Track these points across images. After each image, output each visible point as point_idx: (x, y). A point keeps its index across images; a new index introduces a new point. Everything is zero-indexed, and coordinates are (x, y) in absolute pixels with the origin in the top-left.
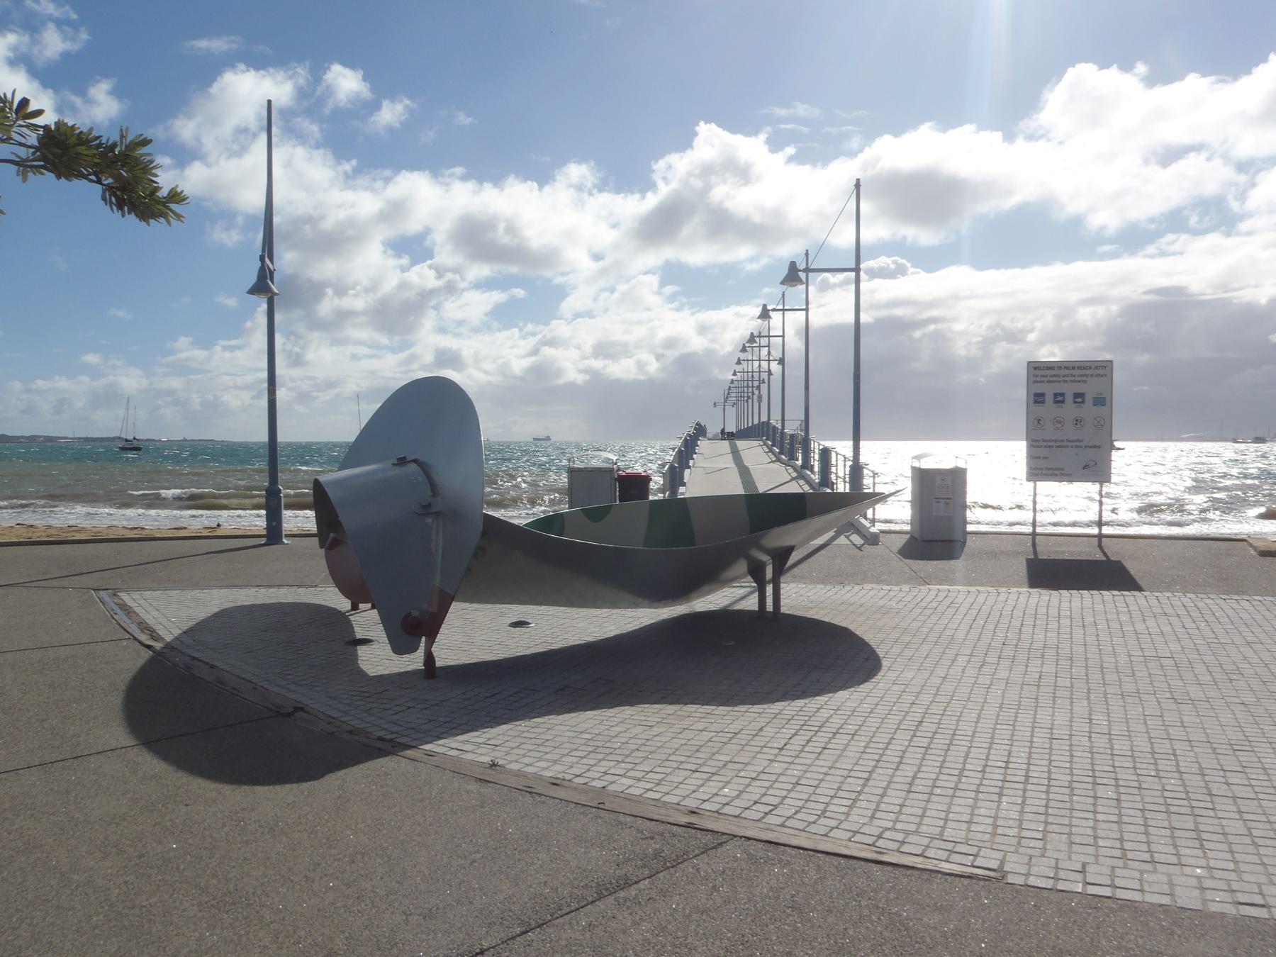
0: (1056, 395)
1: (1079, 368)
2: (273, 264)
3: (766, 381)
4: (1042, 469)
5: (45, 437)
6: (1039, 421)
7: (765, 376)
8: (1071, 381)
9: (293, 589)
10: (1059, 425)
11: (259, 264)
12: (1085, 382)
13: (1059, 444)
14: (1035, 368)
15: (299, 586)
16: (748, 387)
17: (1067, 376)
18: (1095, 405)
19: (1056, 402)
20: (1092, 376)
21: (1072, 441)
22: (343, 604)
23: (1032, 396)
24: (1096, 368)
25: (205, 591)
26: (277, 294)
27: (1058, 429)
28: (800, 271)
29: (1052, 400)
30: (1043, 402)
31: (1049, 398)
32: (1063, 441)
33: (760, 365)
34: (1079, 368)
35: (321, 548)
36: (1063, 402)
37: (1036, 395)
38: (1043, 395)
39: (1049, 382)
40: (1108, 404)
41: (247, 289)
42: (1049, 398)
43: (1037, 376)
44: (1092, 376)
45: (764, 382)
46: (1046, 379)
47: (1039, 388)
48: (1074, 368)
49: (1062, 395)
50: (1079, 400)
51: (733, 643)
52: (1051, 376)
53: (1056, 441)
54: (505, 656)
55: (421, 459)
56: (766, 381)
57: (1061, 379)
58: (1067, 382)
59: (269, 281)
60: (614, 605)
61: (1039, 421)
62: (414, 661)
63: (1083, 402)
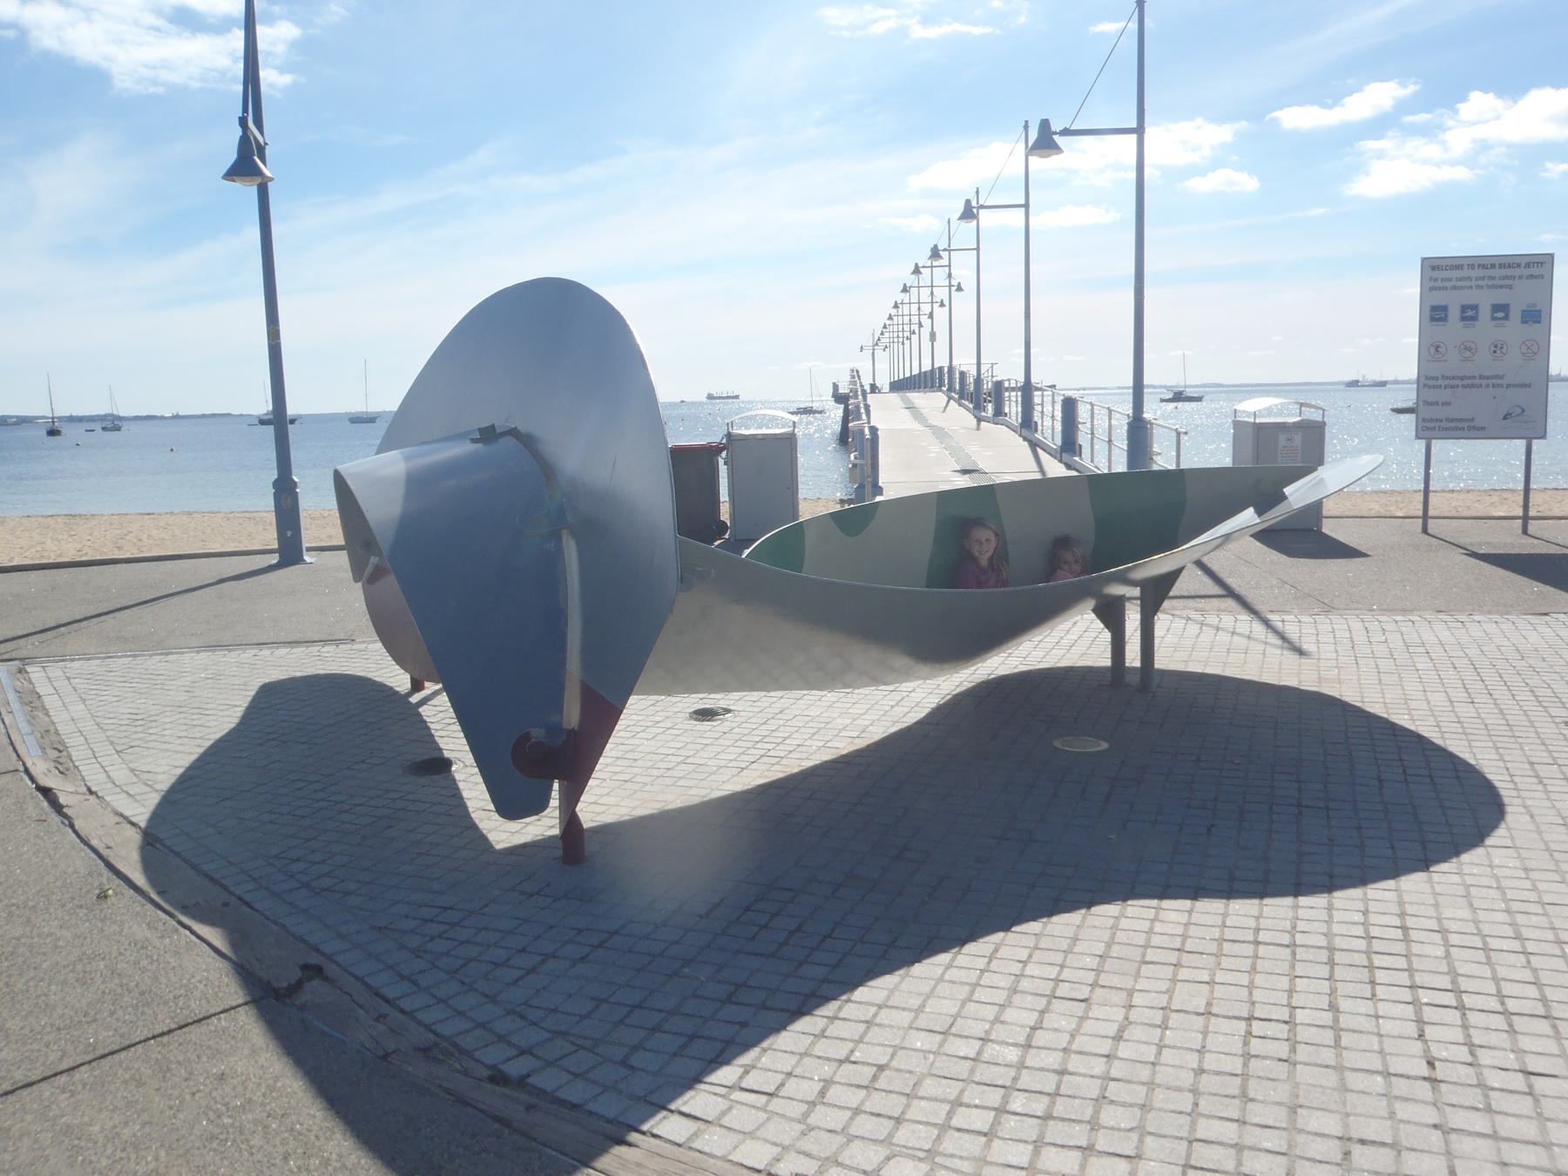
0: (1464, 308)
1: (1501, 266)
2: (263, 135)
3: (917, 331)
4: (1441, 421)
5: (17, 417)
6: (1437, 348)
7: (915, 327)
8: (1489, 287)
9: (314, 649)
10: (1468, 354)
11: (239, 132)
12: (1510, 287)
13: (1466, 382)
14: (1433, 268)
15: (325, 642)
16: (898, 337)
17: (1483, 278)
18: (1523, 322)
19: (1463, 319)
20: (1521, 277)
21: (1488, 378)
22: (400, 680)
23: (1428, 309)
24: (1528, 265)
25: (170, 657)
26: (271, 179)
27: (1466, 359)
28: (1056, 133)
29: (1489, 317)
30: (1445, 319)
31: (1454, 313)
32: (1474, 377)
33: (919, 309)
34: (1501, 266)
35: (356, 581)
36: (1475, 318)
37: (1434, 309)
38: (1444, 308)
39: (1454, 288)
40: (1543, 319)
41: (222, 175)
42: (1454, 313)
43: (1436, 280)
44: (1521, 277)
45: (914, 333)
46: (1449, 284)
47: (1440, 299)
48: (1493, 266)
49: (1475, 307)
50: (1501, 315)
51: (1104, 746)
52: (1461, 279)
53: (1462, 378)
54: (703, 792)
55: (522, 428)
56: (917, 331)
57: (1474, 283)
58: (1482, 287)
59: (256, 158)
60: (876, 681)
61: (1437, 348)
62: (544, 825)
63: (1506, 318)
